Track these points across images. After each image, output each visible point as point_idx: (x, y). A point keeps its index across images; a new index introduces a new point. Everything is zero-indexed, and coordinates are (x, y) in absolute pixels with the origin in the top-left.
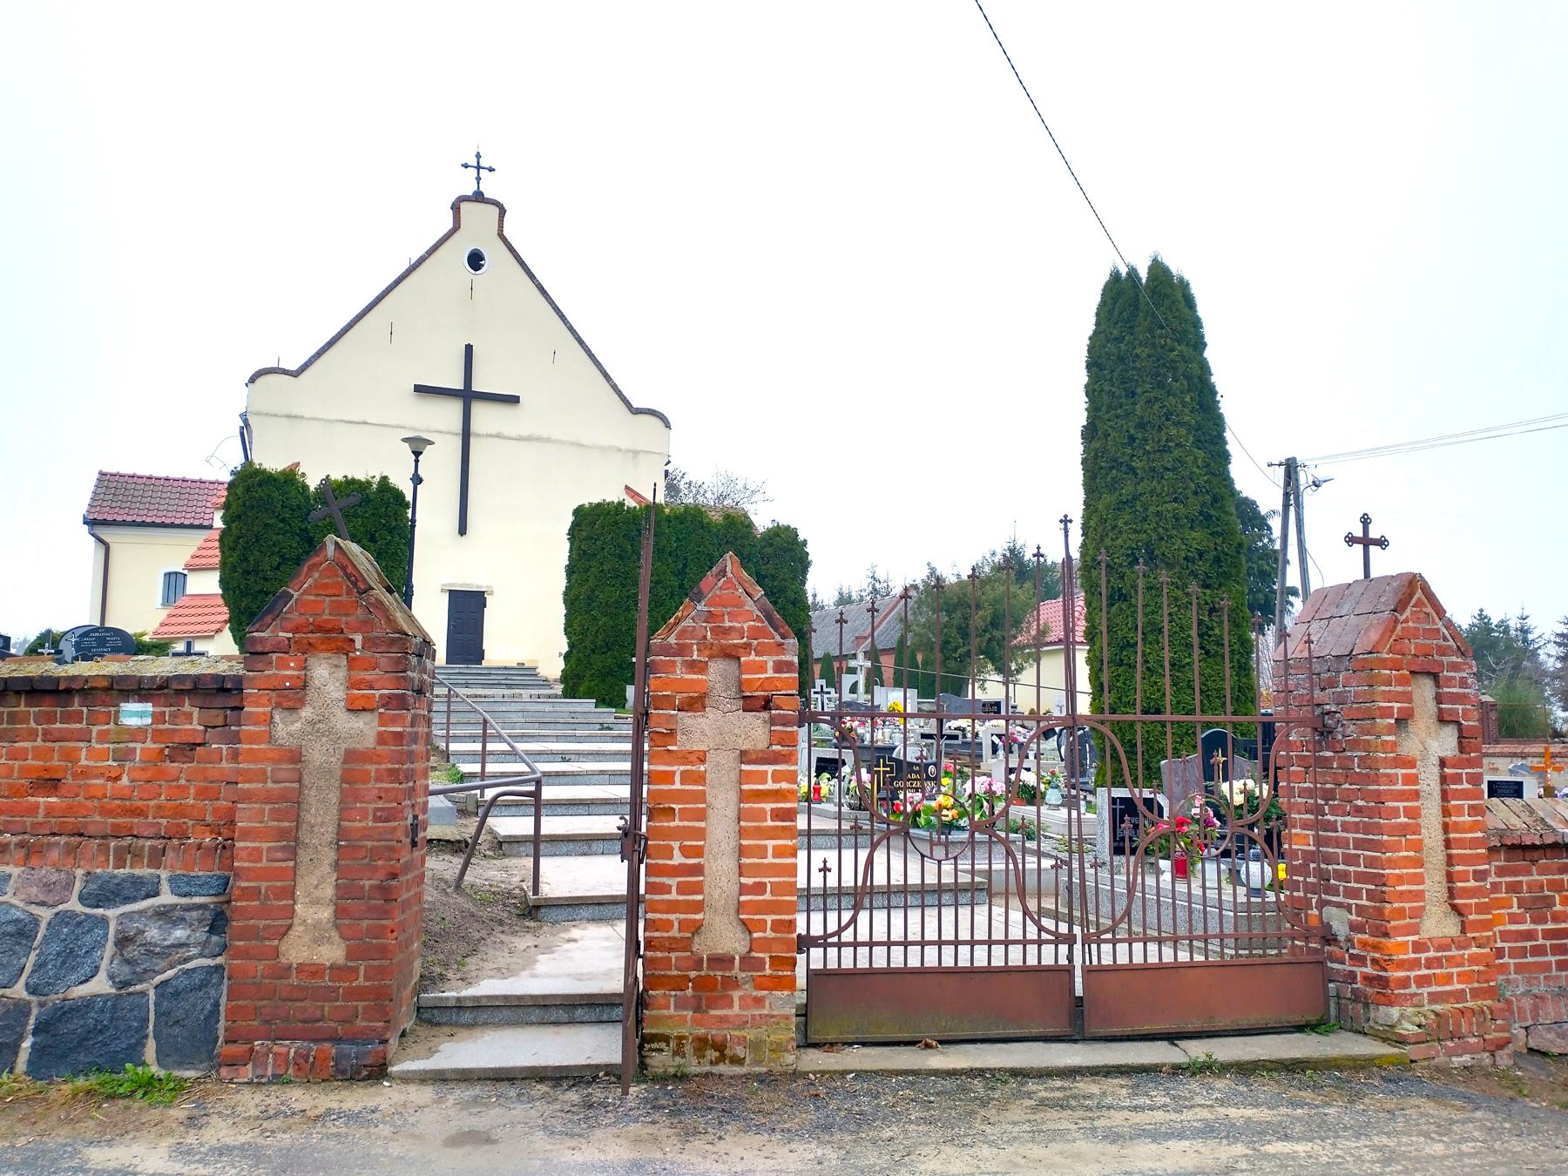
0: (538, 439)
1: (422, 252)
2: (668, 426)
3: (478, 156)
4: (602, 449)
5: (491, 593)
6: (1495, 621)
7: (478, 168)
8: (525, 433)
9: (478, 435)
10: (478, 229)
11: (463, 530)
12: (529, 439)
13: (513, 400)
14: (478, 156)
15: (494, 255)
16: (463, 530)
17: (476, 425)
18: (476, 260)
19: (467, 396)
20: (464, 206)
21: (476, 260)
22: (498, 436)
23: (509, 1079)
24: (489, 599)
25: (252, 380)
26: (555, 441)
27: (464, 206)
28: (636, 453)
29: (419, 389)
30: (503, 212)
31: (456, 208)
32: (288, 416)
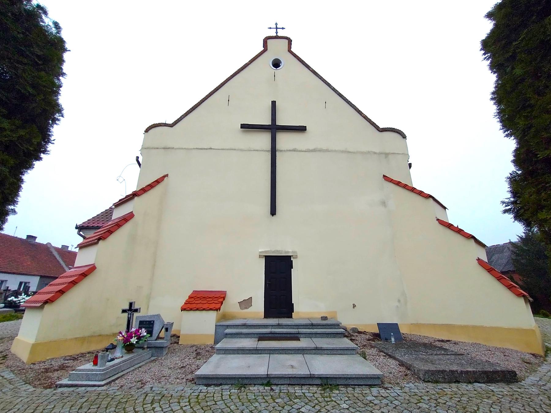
0: (321, 150)
1: (247, 61)
2: (404, 137)
3: (276, 24)
4: (363, 153)
5: (296, 257)
6: (510, 175)
7: (277, 28)
8: (311, 148)
9: (281, 151)
10: (277, 50)
11: (273, 212)
12: (314, 150)
13: (302, 129)
14: (276, 24)
15: (286, 60)
16: (273, 212)
17: (279, 146)
18: (276, 64)
19: (274, 129)
20: (269, 41)
21: (276, 64)
22: (294, 150)
23: (368, 378)
24: (295, 262)
25: (147, 131)
26: (331, 151)
27: (269, 41)
28: (387, 155)
29: (243, 126)
30: (290, 41)
31: (265, 41)
32: (164, 148)
